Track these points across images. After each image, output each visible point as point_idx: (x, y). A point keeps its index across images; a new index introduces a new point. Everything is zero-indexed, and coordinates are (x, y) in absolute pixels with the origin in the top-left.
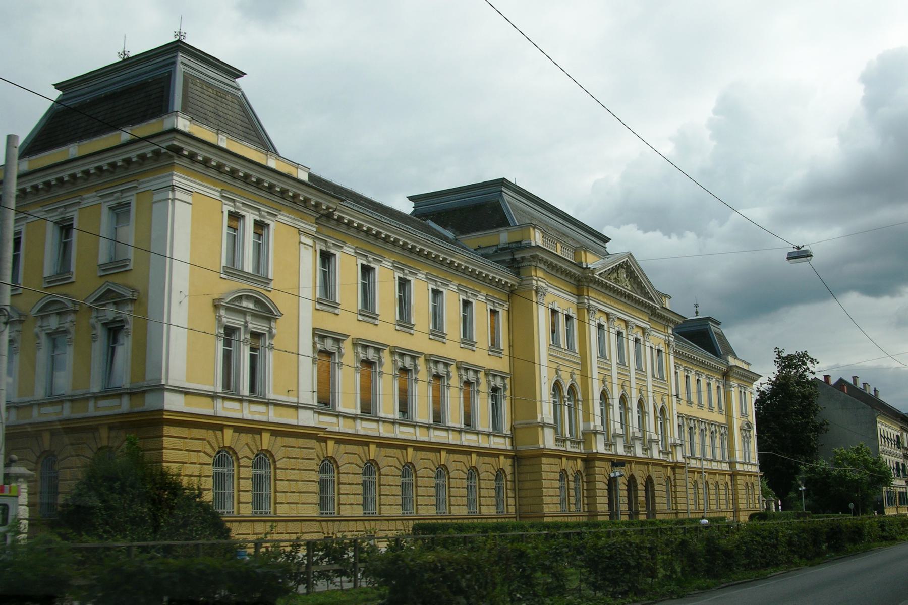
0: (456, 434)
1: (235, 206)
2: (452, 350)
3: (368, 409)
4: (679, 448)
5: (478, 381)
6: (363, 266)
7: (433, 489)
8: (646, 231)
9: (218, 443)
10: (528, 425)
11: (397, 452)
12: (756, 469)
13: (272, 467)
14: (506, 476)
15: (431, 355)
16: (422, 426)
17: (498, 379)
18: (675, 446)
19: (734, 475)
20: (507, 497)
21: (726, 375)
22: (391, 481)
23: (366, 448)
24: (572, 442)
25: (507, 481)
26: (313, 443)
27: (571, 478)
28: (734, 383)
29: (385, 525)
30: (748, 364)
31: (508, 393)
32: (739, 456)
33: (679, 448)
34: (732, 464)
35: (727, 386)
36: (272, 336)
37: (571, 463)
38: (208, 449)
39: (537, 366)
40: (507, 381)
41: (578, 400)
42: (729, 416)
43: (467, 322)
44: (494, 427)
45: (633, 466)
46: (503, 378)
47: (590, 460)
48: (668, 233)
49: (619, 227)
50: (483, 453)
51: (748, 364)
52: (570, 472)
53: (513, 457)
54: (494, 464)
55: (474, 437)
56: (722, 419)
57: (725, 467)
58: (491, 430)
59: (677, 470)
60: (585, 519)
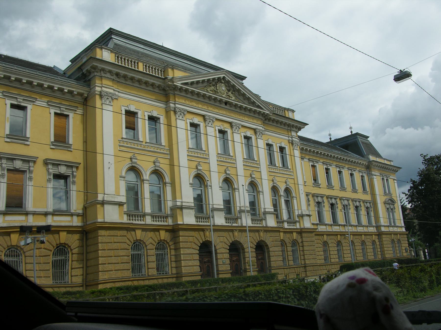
0: (355, 228)
1: (17, 101)
2: (349, 194)
3: (335, 221)
4: (306, 218)
5: (323, 201)
6: (312, 166)
7: (281, 252)
8: (405, 129)
9: (133, 238)
10: (91, 204)
11: (388, 236)
12: (404, 230)
13: (168, 249)
14: (299, 244)
15: (314, 194)
16: (365, 226)
17: (368, 204)
18: (301, 216)
19: (380, 234)
20: (300, 255)
21: (369, 167)
22: (346, 248)
23: (292, 234)
24: (288, 223)
25: (299, 246)
26: (124, 233)
27: (396, 243)
28: (375, 172)
29: (333, 266)
30: (390, 161)
31: (372, 209)
32: (383, 221)
33: (306, 218)
34: (378, 227)
35: (370, 175)
36: (31, 172)
37: (395, 236)
38: (128, 241)
39: (99, 157)
40: (371, 204)
41: (281, 196)
42: (373, 194)
43: (341, 180)
44: (358, 223)
45: (261, 234)
46: (370, 203)
47: (174, 230)
48: (416, 128)
49: (393, 128)
50: (366, 234)
51: (390, 161)
52: (395, 240)
53: (378, 235)
54: (322, 239)
55: (338, 227)
56: (368, 197)
57: (372, 230)
58: (318, 222)
59: (304, 235)
60: (174, 280)
